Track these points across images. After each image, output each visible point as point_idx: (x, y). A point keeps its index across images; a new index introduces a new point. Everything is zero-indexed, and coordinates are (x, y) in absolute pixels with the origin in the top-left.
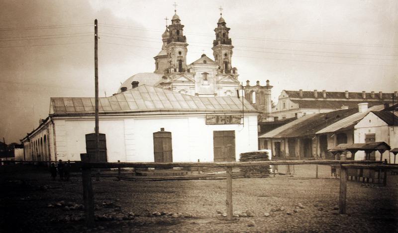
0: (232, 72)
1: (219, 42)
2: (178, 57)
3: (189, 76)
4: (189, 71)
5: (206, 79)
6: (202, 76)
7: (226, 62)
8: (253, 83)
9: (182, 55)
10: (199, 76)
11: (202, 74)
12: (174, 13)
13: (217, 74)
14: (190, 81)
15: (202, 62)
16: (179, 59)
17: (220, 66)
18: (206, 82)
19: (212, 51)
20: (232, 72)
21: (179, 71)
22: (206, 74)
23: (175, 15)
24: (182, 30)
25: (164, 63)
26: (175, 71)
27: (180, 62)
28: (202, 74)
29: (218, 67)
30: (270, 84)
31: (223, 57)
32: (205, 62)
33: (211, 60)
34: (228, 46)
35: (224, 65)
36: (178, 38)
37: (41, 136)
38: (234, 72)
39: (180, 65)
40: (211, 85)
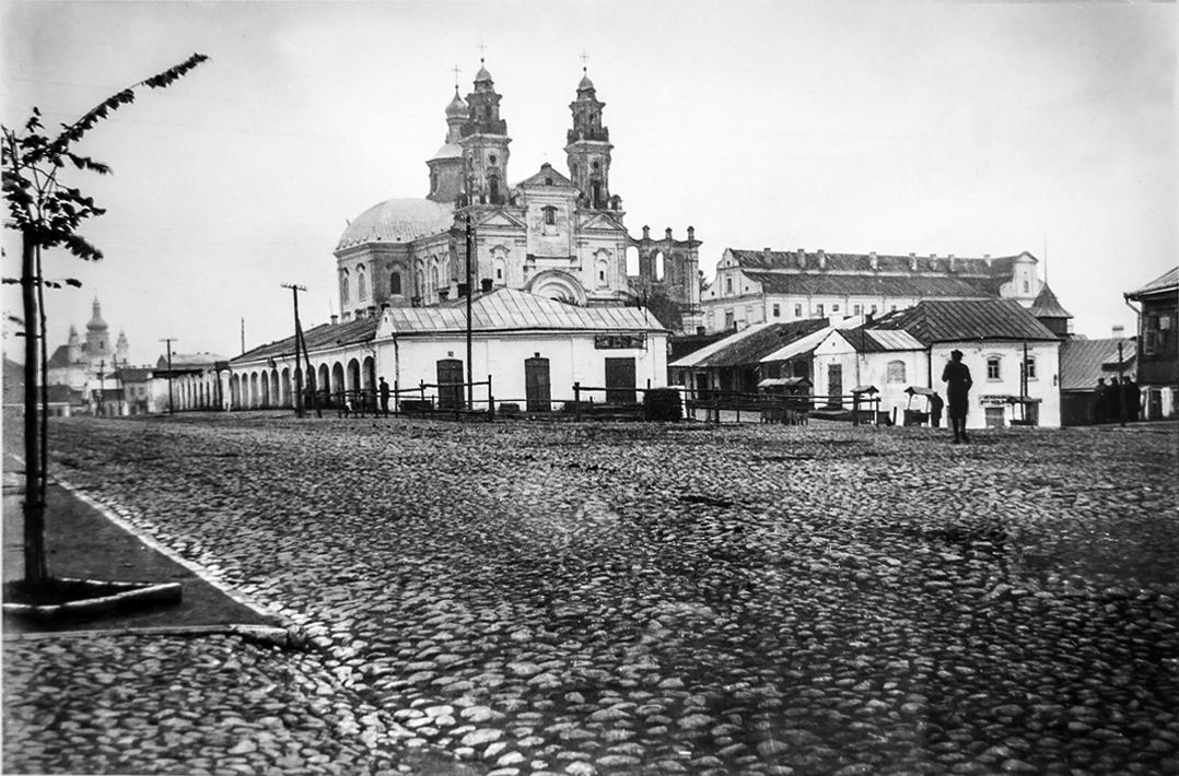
0: (610, 205)
4: (512, 202)
5: (551, 222)
8: (657, 234)
9: (497, 164)
10: (535, 214)
14: (515, 225)
15: (543, 180)
18: (551, 229)
19: (565, 155)
20: (610, 205)
26: (483, 201)
33: (561, 177)
40: (564, 236)
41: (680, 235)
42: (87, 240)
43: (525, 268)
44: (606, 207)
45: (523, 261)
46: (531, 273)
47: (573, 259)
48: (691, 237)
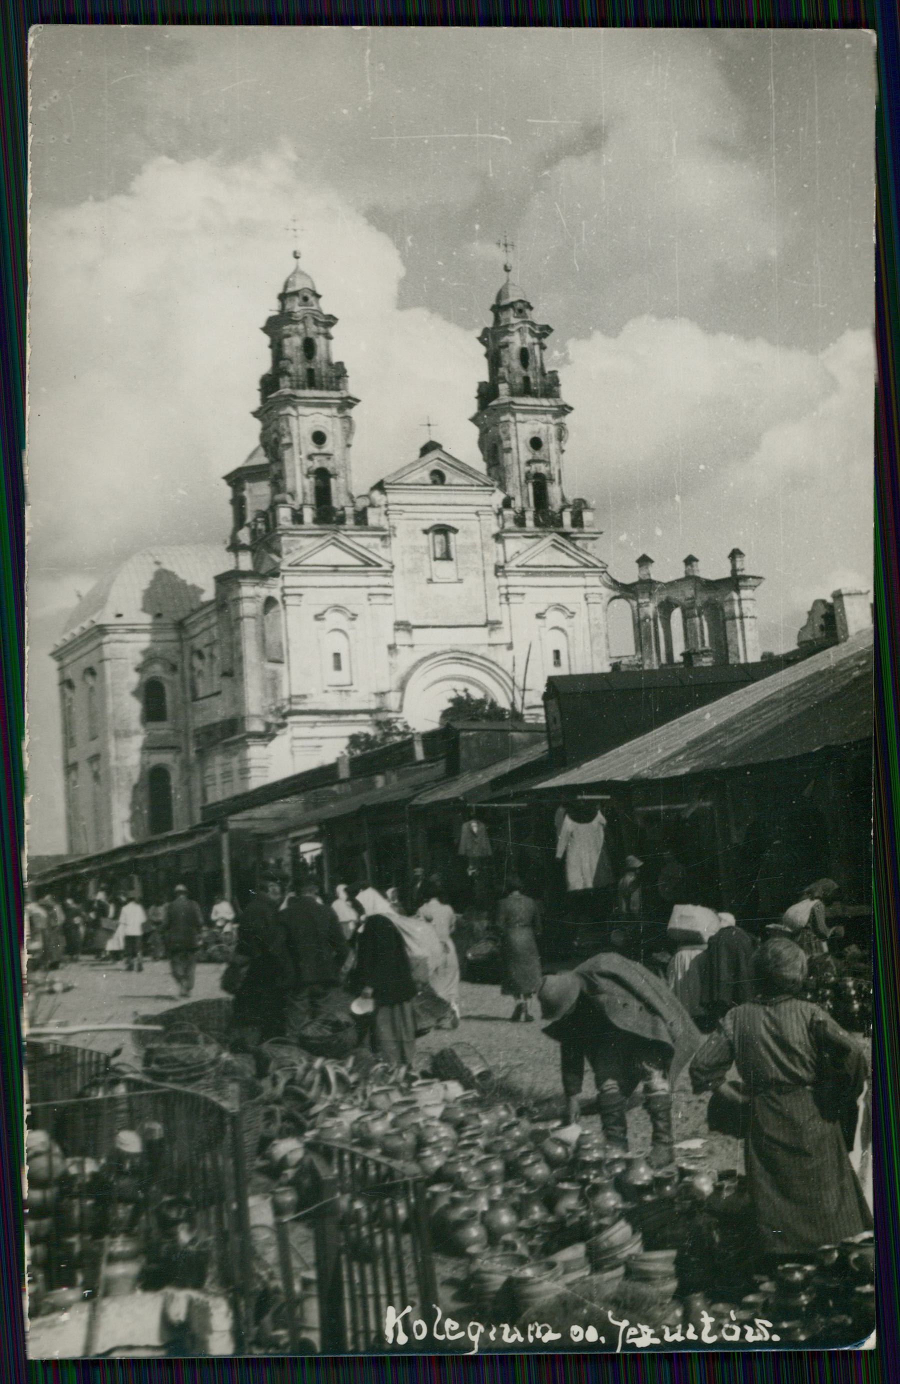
0: (567, 518)
1: (503, 388)
2: (310, 457)
3: (366, 542)
4: (361, 518)
5: (447, 556)
6: (425, 541)
7: (538, 475)
9: (328, 447)
10: (408, 545)
11: (426, 532)
12: (290, 265)
13: (496, 529)
14: (367, 563)
15: (424, 475)
16: (316, 464)
17: (511, 491)
18: (444, 569)
19: (474, 432)
20: (567, 518)
21: (315, 521)
22: (443, 530)
23: (297, 272)
24: (328, 337)
25: (258, 494)
26: (297, 518)
27: (323, 477)
28: (426, 532)
29: (498, 498)
30: (747, 566)
31: (526, 454)
32: (438, 477)
33: (464, 469)
34: (545, 402)
35: (530, 488)
36: (310, 372)
37: (278, 839)
38: (577, 521)
39: (323, 494)
40: (473, 581)
41: (714, 568)
42: (145, 585)
43: (392, 648)
44: (560, 523)
45: (389, 636)
46: (405, 659)
47: (492, 625)
48: (734, 570)
